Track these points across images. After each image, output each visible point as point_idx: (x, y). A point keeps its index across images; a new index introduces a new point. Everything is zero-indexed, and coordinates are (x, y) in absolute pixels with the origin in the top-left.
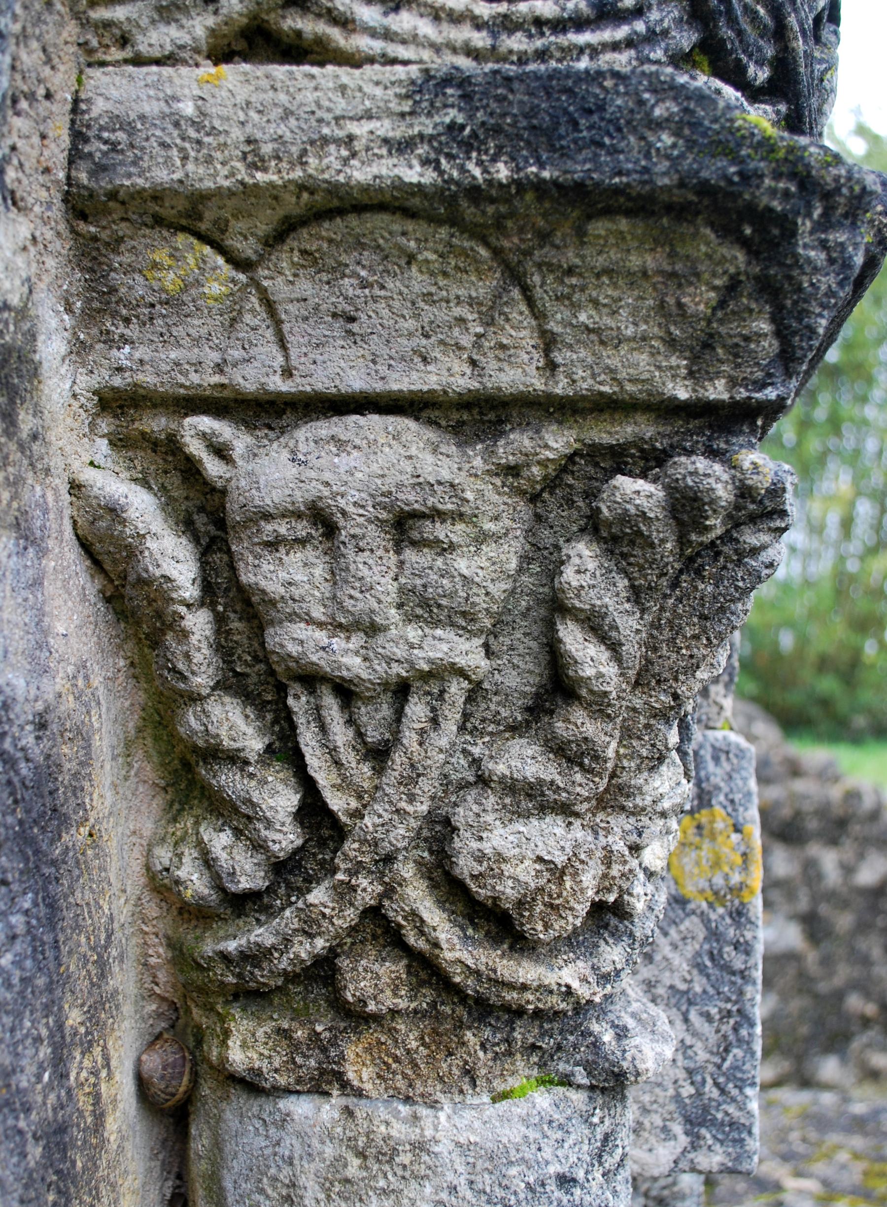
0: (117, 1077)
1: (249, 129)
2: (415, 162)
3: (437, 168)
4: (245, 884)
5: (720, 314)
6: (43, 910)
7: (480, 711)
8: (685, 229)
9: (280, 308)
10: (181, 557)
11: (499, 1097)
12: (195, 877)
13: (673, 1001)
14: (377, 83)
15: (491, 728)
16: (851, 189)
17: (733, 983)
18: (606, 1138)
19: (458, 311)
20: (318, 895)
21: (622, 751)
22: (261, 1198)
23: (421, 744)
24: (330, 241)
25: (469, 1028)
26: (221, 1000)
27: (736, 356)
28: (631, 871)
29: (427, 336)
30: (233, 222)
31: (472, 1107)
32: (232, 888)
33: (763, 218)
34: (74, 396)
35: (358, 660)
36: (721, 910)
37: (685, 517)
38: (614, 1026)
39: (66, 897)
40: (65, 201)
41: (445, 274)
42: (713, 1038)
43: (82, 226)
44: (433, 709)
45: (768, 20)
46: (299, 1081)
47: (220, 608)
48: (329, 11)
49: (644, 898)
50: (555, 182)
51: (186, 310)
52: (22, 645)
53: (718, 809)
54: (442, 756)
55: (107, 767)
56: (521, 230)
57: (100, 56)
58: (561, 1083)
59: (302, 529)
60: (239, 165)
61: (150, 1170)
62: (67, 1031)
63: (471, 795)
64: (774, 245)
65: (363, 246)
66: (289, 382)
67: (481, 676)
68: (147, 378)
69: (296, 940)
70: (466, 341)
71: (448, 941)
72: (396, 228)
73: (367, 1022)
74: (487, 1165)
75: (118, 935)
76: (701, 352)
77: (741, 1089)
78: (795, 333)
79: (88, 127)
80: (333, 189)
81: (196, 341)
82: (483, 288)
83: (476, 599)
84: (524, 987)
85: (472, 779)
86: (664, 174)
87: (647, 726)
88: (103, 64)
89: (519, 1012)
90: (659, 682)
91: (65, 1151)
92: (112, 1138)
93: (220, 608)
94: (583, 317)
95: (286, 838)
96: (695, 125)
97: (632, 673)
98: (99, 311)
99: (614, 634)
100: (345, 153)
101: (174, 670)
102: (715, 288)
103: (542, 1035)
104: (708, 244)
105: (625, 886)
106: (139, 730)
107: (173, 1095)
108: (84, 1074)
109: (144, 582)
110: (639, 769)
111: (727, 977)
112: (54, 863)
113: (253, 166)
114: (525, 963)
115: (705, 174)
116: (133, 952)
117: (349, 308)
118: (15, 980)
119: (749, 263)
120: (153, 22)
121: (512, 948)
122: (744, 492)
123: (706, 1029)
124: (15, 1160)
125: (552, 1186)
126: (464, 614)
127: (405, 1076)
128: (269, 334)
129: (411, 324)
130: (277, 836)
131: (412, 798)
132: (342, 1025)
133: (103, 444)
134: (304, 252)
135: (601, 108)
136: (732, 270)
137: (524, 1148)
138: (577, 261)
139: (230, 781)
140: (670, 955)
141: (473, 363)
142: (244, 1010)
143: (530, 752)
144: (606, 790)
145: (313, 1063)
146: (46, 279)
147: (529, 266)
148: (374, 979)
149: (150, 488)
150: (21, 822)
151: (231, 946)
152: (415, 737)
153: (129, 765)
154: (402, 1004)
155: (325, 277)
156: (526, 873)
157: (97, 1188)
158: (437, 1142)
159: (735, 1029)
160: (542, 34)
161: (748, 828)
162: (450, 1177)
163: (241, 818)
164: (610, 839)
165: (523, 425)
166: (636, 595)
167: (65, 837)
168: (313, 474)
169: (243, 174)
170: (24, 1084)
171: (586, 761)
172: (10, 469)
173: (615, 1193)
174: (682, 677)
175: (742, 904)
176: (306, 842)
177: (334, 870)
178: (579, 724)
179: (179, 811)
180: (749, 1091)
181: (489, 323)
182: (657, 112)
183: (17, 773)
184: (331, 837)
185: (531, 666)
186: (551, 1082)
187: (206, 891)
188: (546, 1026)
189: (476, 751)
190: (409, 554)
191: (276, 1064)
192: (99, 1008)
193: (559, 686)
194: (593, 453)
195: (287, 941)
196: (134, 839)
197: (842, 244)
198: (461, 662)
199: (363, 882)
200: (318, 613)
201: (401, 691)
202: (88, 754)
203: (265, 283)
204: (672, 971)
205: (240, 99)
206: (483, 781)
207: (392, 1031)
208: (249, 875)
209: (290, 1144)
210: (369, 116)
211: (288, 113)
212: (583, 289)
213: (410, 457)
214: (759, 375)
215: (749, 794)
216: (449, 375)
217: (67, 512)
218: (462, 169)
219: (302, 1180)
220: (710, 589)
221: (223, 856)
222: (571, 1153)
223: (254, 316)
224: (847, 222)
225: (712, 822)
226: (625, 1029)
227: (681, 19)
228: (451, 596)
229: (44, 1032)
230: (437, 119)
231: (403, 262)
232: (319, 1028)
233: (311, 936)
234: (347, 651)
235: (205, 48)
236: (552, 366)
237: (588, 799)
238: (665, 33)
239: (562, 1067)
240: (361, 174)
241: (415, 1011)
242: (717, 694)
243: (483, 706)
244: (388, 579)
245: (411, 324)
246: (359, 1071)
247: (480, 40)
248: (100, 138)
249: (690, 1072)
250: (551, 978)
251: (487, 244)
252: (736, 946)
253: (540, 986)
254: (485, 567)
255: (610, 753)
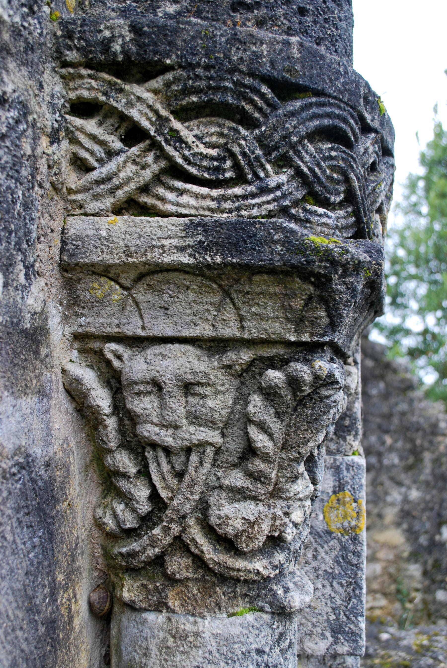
0: (80, 602)
1: (126, 241)
2: (186, 255)
3: (195, 258)
4: (128, 525)
5: (306, 309)
6: (47, 536)
7: (221, 458)
8: (289, 278)
9: (140, 304)
10: (104, 397)
11: (231, 615)
12: (110, 522)
13: (326, 577)
14: (173, 225)
15: (225, 465)
16: (354, 262)
17: (353, 570)
18: (281, 635)
19: (206, 307)
20: (157, 531)
21: (279, 474)
22: (135, 654)
23: (196, 472)
24: (158, 281)
25: (218, 586)
26: (121, 572)
27: (313, 324)
28: (285, 523)
29: (196, 316)
30: (121, 274)
31: (219, 619)
32: (124, 527)
33: (318, 276)
34: (64, 335)
35: (171, 439)
36: (347, 537)
37: (294, 386)
38: (283, 587)
39: (57, 530)
40: (59, 266)
41: (201, 293)
42: (344, 594)
43: (66, 274)
44: (201, 458)
45: (340, 177)
46: (150, 606)
47: (121, 415)
48: (157, 195)
49: (290, 534)
50: (238, 263)
51: (105, 304)
52: (40, 436)
53: (347, 491)
54: (204, 477)
55: (77, 477)
56: (228, 279)
57: (72, 212)
58: (260, 610)
59: (149, 388)
60: (122, 255)
61: (95, 643)
62: (57, 583)
63: (216, 492)
64: (324, 284)
65: (170, 283)
66: (144, 332)
67: (219, 445)
68: (91, 329)
69: (148, 548)
70: (210, 318)
71: (207, 550)
72: (181, 277)
73: (177, 582)
74: (225, 643)
75: (81, 544)
76: (299, 323)
77: (356, 617)
78: (334, 316)
79: (68, 239)
80: (157, 264)
81: (109, 316)
82: (215, 299)
83: (216, 416)
84: (239, 570)
85: (217, 485)
86: (278, 261)
87: (289, 465)
88: (73, 215)
89: (238, 580)
90: (292, 448)
91: (55, 630)
92: (77, 627)
93: (121, 415)
94: (253, 310)
95: (144, 507)
96: (290, 242)
97: (280, 445)
98: (73, 304)
99: (269, 430)
100: (161, 251)
101: (102, 440)
102: (303, 299)
103: (249, 590)
104: (298, 284)
105: (282, 529)
106: (91, 461)
107: (103, 610)
108: (64, 600)
109: (90, 407)
110: (286, 481)
111: (350, 567)
112: (52, 517)
113: (128, 256)
114: (239, 560)
115: (293, 261)
116: (88, 551)
117: (166, 305)
118: (35, 563)
119: (315, 290)
120: (91, 200)
121: (235, 554)
122: (317, 377)
123: (340, 590)
124: (33, 631)
125: (253, 654)
126: (211, 422)
127: (192, 605)
128: (137, 314)
129: (189, 311)
130: (141, 507)
131: (192, 494)
132: (167, 583)
133: (75, 352)
134: (148, 285)
135: (255, 236)
136: (309, 293)
137: (241, 637)
138: (250, 290)
139: (123, 484)
140: (325, 557)
141: (213, 326)
142: (130, 576)
143: (239, 476)
144: (274, 490)
145: (155, 598)
146: (51, 297)
147: (232, 291)
148: (178, 565)
149: (94, 369)
150: (38, 503)
151: (124, 550)
152: (193, 469)
153: (87, 475)
154: (190, 575)
155: (156, 293)
156: (238, 524)
157: (69, 647)
158: (204, 632)
159: (354, 590)
160: (238, 201)
161: (360, 501)
162: (209, 647)
163: (127, 499)
164: (276, 510)
165: (232, 349)
166: (278, 415)
167: (57, 507)
168: (153, 368)
169: (124, 259)
170: (38, 602)
171: (262, 479)
172: (37, 371)
173: (285, 659)
174: (301, 446)
175: (356, 534)
176: (153, 509)
177: (163, 521)
178: (259, 465)
179: (107, 494)
180: (360, 618)
181: (219, 311)
182: (275, 237)
183: (37, 485)
184: (163, 507)
185: (240, 441)
186: (255, 610)
187: (115, 528)
188: (251, 586)
189: (219, 474)
190: (190, 398)
191: (141, 598)
192: (72, 574)
193: (250, 451)
194: (262, 359)
195: (145, 549)
196: (89, 505)
197: (352, 282)
198: (211, 440)
199: (173, 526)
200: (156, 420)
201: (188, 451)
202: (68, 474)
203: (134, 296)
204: (326, 564)
205: (123, 230)
206: (221, 487)
207: (187, 587)
208: (130, 522)
209: (147, 632)
210: (170, 237)
211: (140, 236)
212: (253, 300)
213: (189, 362)
214: (322, 332)
215: (361, 485)
216: (204, 330)
217: (61, 381)
218: (204, 258)
219: (151, 647)
220: (310, 412)
221: (121, 514)
222: (264, 639)
223: (131, 307)
224: (355, 273)
225: (344, 498)
226: (288, 588)
227: (298, 186)
228: (206, 415)
229: (47, 583)
230: (195, 239)
231: (185, 289)
232: (158, 584)
233: (154, 547)
234: (166, 435)
235: (110, 210)
236: (243, 327)
237: (264, 494)
238: (291, 193)
239: (260, 604)
240: (167, 259)
241: (196, 579)
242: (350, 440)
243: (222, 456)
244: (182, 408)
245: (189, 311)
246: (174, 602)
247: (213, 205)
248: (72, 244)
249: (334, 609)
250: (250, 566)
251: (216, 283)
252: (354, 553)
253: (245, 570)
254: (218, 404)
255: (273, 475)
